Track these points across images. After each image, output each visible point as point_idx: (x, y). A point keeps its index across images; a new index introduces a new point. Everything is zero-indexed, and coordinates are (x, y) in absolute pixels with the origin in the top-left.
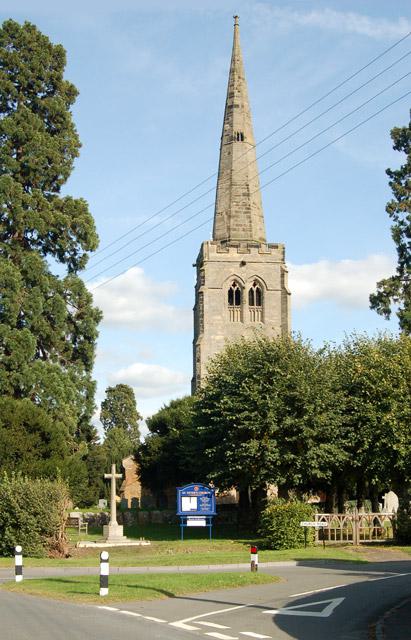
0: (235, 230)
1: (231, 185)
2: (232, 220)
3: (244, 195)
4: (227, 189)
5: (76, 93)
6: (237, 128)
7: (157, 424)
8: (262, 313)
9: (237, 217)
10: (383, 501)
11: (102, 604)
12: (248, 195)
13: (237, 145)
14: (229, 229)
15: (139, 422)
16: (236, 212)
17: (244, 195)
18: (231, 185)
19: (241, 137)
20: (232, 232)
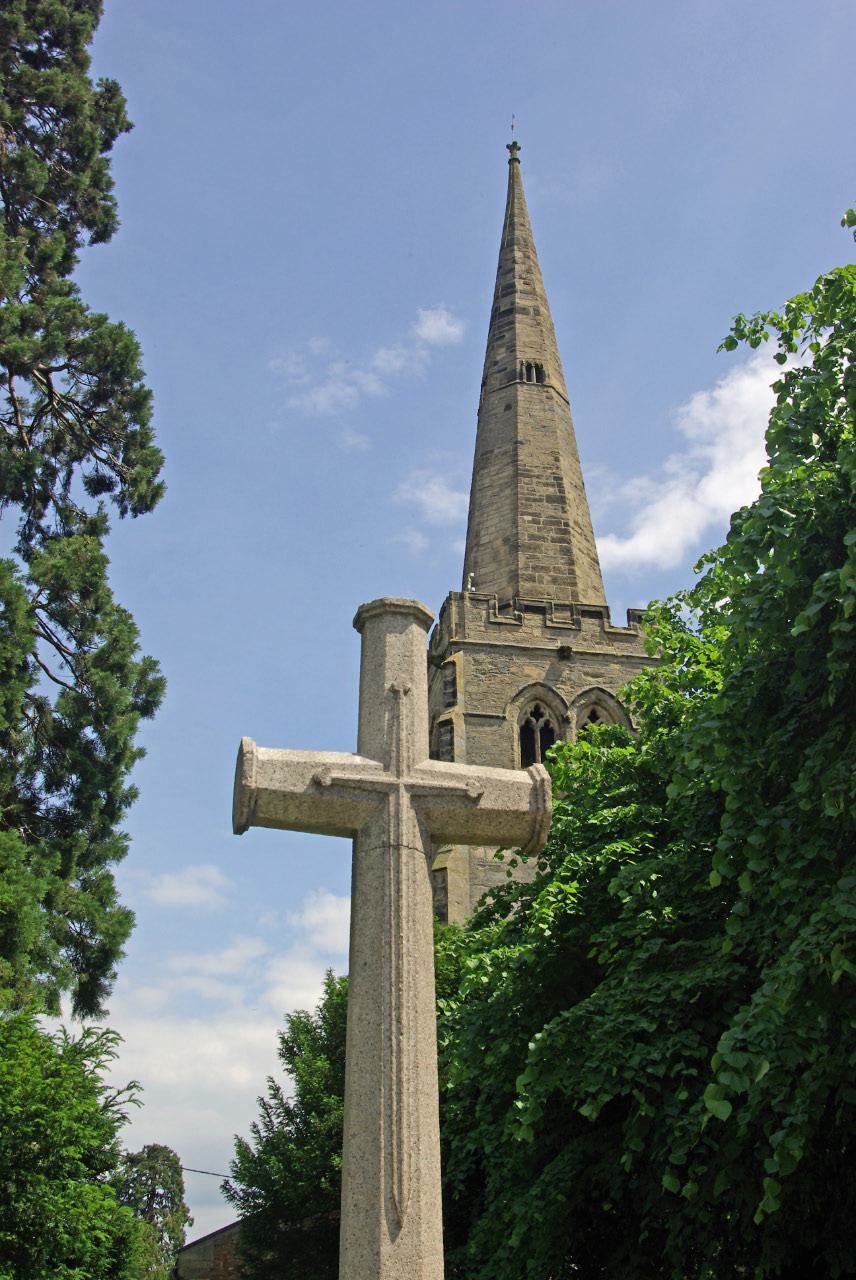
0: (531, 579)
1: (516, 475)
2: (522, 557)
3: (550, 499)
4: (506, 485)
5: (113, 183)
6: (524, 355)
7: (333, 780)
8: (539, 270)
9: (536, 548)
10: (291, 1071)
11: (396, 1038)
12: (560, 500)
13: (523, 392)
14: (514, 577)
15: (623, 1094)
16: (532, 537)
17: (550, 499)
18: (516, 475)
19: (536, 373)
20: (525, 586)
